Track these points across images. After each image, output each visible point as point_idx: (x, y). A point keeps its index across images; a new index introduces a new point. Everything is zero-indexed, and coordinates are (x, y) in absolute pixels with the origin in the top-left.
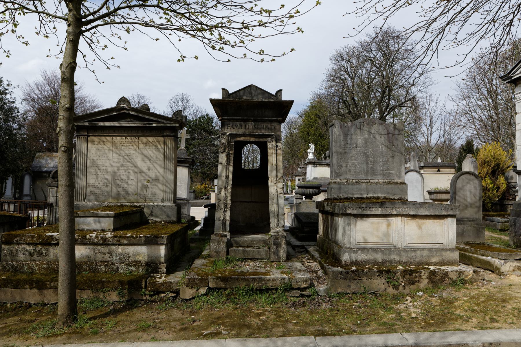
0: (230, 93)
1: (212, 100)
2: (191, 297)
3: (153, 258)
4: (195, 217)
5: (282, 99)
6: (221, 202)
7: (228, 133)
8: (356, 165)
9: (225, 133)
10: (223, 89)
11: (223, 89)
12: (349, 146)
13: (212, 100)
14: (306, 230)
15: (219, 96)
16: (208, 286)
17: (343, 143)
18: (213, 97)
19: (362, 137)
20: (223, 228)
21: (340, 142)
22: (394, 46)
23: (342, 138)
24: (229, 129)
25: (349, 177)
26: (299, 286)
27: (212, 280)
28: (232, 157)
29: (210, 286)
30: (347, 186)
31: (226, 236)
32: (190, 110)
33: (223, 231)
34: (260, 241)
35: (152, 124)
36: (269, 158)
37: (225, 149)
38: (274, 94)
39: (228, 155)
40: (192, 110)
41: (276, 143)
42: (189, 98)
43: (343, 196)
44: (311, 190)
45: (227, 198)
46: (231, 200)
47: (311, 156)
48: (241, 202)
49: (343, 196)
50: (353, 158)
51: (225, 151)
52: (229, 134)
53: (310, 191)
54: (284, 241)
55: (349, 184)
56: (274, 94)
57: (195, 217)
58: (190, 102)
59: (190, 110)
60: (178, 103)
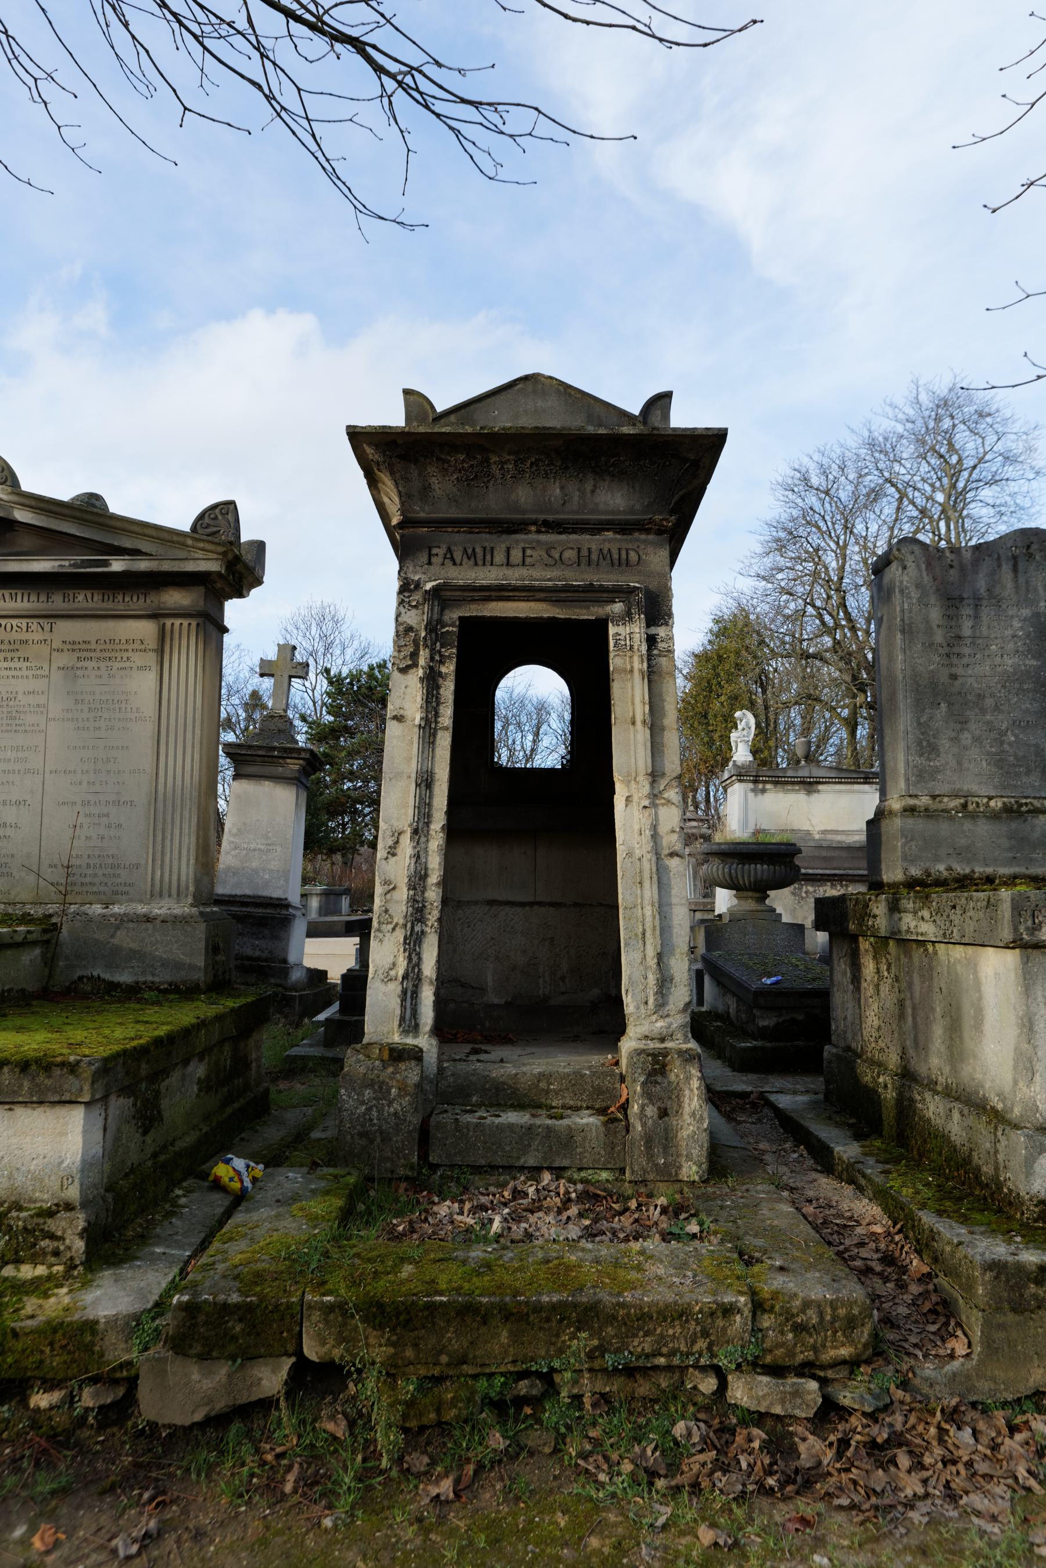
0: (440, 408)
1: (357, 436)
2: (198, 1417)
3: (19, 1180)
4: (325, 973)
5: (672, 425)
6: (396, 895)
7: (429, 586)
8: (1003, 733)
9: (418, 585)
10: (407, 392)
11: (407, 392)
12: (966, 651)
13: (357, 436)
14: (762, 1023)
15: (395, 417)
16: (299, 1353)
17: (939, 637)
18: (364, 420)
19: (1026, 612)
20: (402, 1019)
21: (929, 631)
22: (967, 443)
23: (935, 614)
24: (434, 569)
25: (975, 788)
26: (810, 1355)
27: (316, 1316)
28: (448, 690)
29: (312, 1351)
30: (968, 825)
31: (416, 1055)
32: (343, 653)
33: (405, 1032)
34: (575, 1081)
35: (106, 563)
36: (617, 689)
37: (414, 655)
38: (636, 411)
39: (432, 681)
40: (349, 652)
41: (648, 626)
42: (340, 616)
43: (949, 869)
44: (766, 864)
45: (425, 876)
46: (445, 883)
47: (742, 755)
48: (491, 903)
49: (949, 869)
50: (989, 702)
51: (415, 665)
52: (436, 589)
53: (761, 870)
54: (695, 1083)
55: (973, 816)
56: (636, 411)
57: (325, 973)
58: (343, 628)
59: (343, 653)
60: (309, 628)
